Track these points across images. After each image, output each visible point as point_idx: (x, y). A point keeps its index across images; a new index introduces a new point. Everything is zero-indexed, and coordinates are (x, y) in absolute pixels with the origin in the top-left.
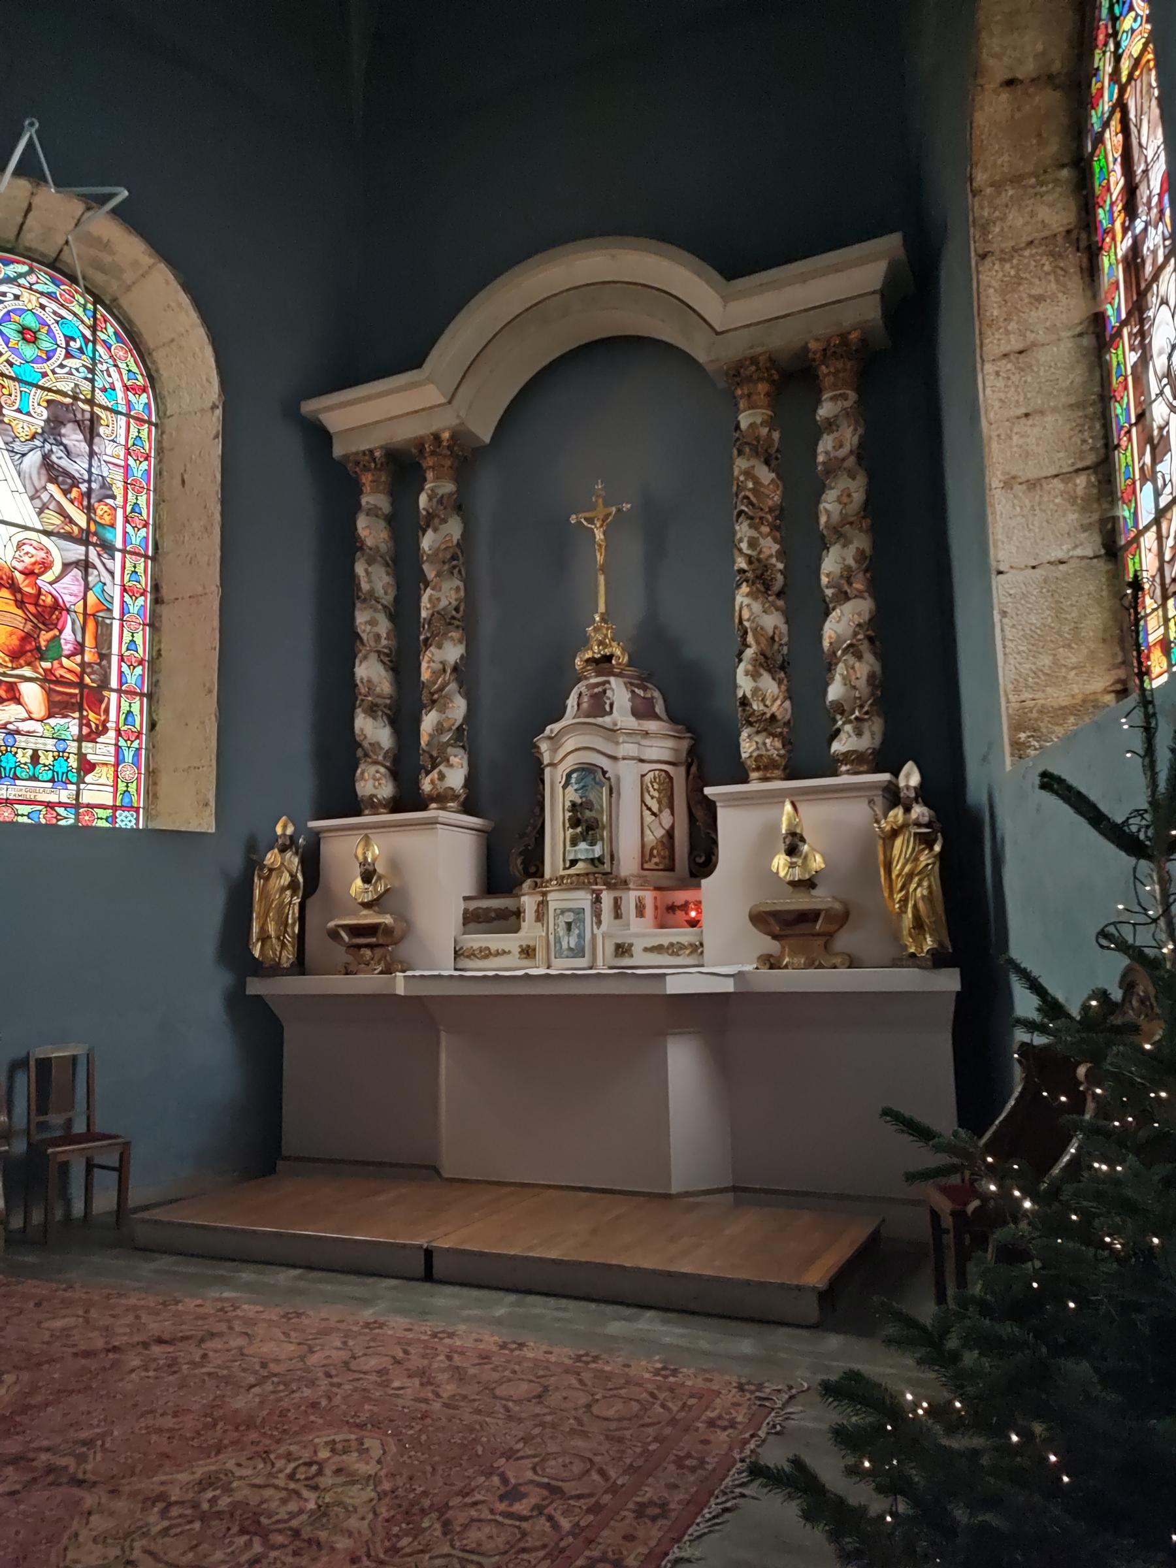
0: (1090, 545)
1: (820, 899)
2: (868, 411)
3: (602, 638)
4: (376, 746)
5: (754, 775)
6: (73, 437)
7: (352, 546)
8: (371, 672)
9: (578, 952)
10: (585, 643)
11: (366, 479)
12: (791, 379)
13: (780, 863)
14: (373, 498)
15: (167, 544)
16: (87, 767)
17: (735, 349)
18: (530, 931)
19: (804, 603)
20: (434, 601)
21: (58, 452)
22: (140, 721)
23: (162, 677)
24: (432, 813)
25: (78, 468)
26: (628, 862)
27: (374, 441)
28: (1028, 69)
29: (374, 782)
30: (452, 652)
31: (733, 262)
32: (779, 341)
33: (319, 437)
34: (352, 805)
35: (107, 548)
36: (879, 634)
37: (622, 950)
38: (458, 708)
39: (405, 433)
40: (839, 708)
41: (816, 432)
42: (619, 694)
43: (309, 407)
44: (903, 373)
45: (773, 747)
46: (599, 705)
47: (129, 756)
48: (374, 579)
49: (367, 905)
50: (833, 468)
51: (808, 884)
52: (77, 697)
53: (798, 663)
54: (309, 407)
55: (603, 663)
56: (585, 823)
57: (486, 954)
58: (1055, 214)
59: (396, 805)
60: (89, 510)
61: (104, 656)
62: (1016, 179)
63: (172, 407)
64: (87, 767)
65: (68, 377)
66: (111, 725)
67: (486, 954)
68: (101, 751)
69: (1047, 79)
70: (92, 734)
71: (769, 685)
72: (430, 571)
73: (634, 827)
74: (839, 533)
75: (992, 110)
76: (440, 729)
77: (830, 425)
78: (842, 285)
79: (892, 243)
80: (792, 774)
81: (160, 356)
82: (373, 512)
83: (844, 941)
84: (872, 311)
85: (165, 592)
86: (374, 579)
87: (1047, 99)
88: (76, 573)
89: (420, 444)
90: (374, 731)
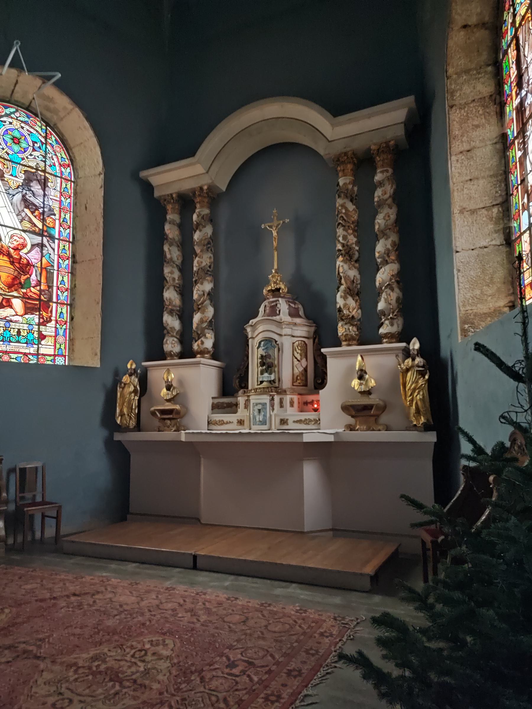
0: (499, 239)
1: (373, 400)
2: (398, 178)
3: (275, 280)
4: (173, 328)
5: (344, 343)
6: (36, 187)
7: (162, 237)
8: (171, 295)
9: (263, 423)
10: (268, 283)
11: (169, 207)
12: (363, 162)
13: (355, 383)
14: (172, 216)
15: (78, 236)
16: (42, 337)
17: (338, 148)
18: (242, 413)
19: (368, 266)
20: (199, 263)
21: (29, 194)
22: (66, 317)
23: (77, 297)
24: (198, 359)
25: (38, 201)
26: (286, 382)
27: (173, 190)
28: (473, 20)
29: (171, 345)
30: (208, 286)
31: (337, 109)
32: (358, 145)
33: (147, 188)
34: (162, 356)
35: (52, 238)
36: (402, 279)
37: (283, 422)
38: (210, 312)
39: (187, 186)
40: (383, 313)
41: (374, 187)
42: (283, 306)
43: (143, 174)
44: (414, 159)
45: (353, 330)
46: (274, 311)
47: (61, 332)
48: (172, 253)
49: (168, 401)
50: (382, 204)
51: (368, 393)
52: (38, 305)
53: (365, 293)
54: (143, 174)
55: (276, 292)
56: (267, 364)
57: (222, 423)
58: (484, 87)
59: (181, 356)
60: (43, 221)
61: (50, 287)
62: (467, 71)
63: (81, 174)
64: (42, 337)
65: (34, 160)
66: (53, 318)
67: (222, 423)
68: (49, 330)
69: (483, 25)
70: (44, 322)
71: (351, 302)
72: (198, 249)
73: (289, 367)
74: (384, 234)
75: (457, 39)
76: (202, 321)
77: (381, 184)
78: (386, 120)
79: (410, 100)
80: (361, 343)
81: (76, 151)
82: (172, 222)
83: (384, 418)
84: (400, 132)
85: (78, 258)
86: (172, 253)
87: (482, 34)
88: (37, 249)
89: (193, 191)
90: (172, 322)
